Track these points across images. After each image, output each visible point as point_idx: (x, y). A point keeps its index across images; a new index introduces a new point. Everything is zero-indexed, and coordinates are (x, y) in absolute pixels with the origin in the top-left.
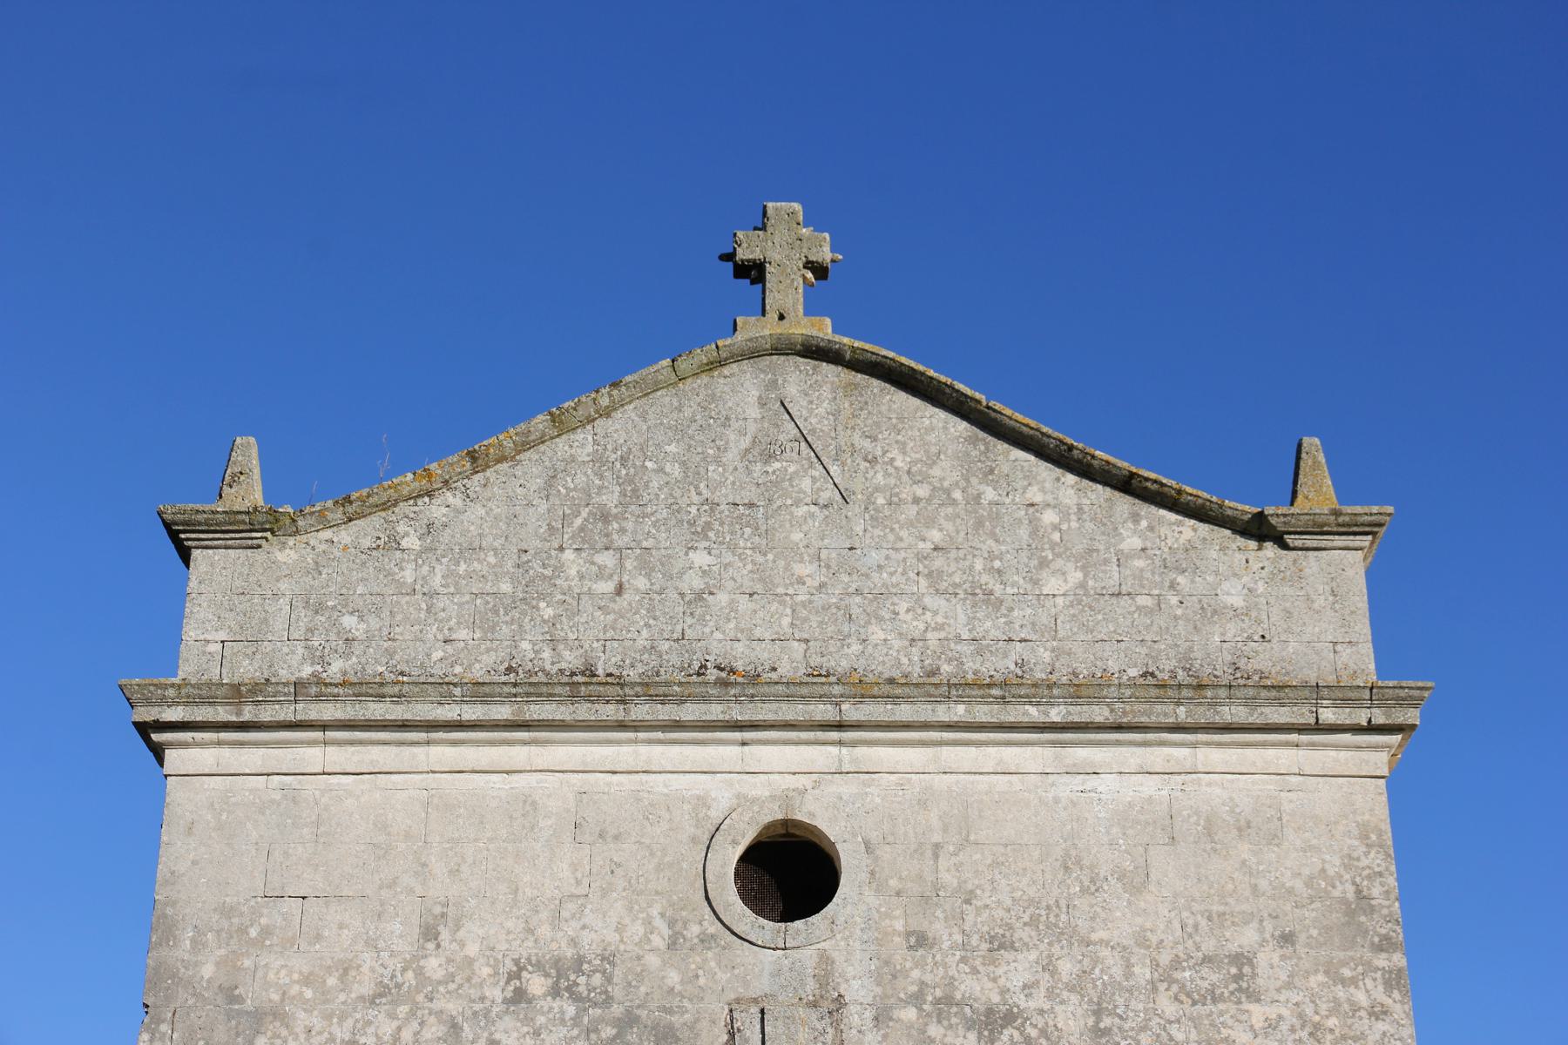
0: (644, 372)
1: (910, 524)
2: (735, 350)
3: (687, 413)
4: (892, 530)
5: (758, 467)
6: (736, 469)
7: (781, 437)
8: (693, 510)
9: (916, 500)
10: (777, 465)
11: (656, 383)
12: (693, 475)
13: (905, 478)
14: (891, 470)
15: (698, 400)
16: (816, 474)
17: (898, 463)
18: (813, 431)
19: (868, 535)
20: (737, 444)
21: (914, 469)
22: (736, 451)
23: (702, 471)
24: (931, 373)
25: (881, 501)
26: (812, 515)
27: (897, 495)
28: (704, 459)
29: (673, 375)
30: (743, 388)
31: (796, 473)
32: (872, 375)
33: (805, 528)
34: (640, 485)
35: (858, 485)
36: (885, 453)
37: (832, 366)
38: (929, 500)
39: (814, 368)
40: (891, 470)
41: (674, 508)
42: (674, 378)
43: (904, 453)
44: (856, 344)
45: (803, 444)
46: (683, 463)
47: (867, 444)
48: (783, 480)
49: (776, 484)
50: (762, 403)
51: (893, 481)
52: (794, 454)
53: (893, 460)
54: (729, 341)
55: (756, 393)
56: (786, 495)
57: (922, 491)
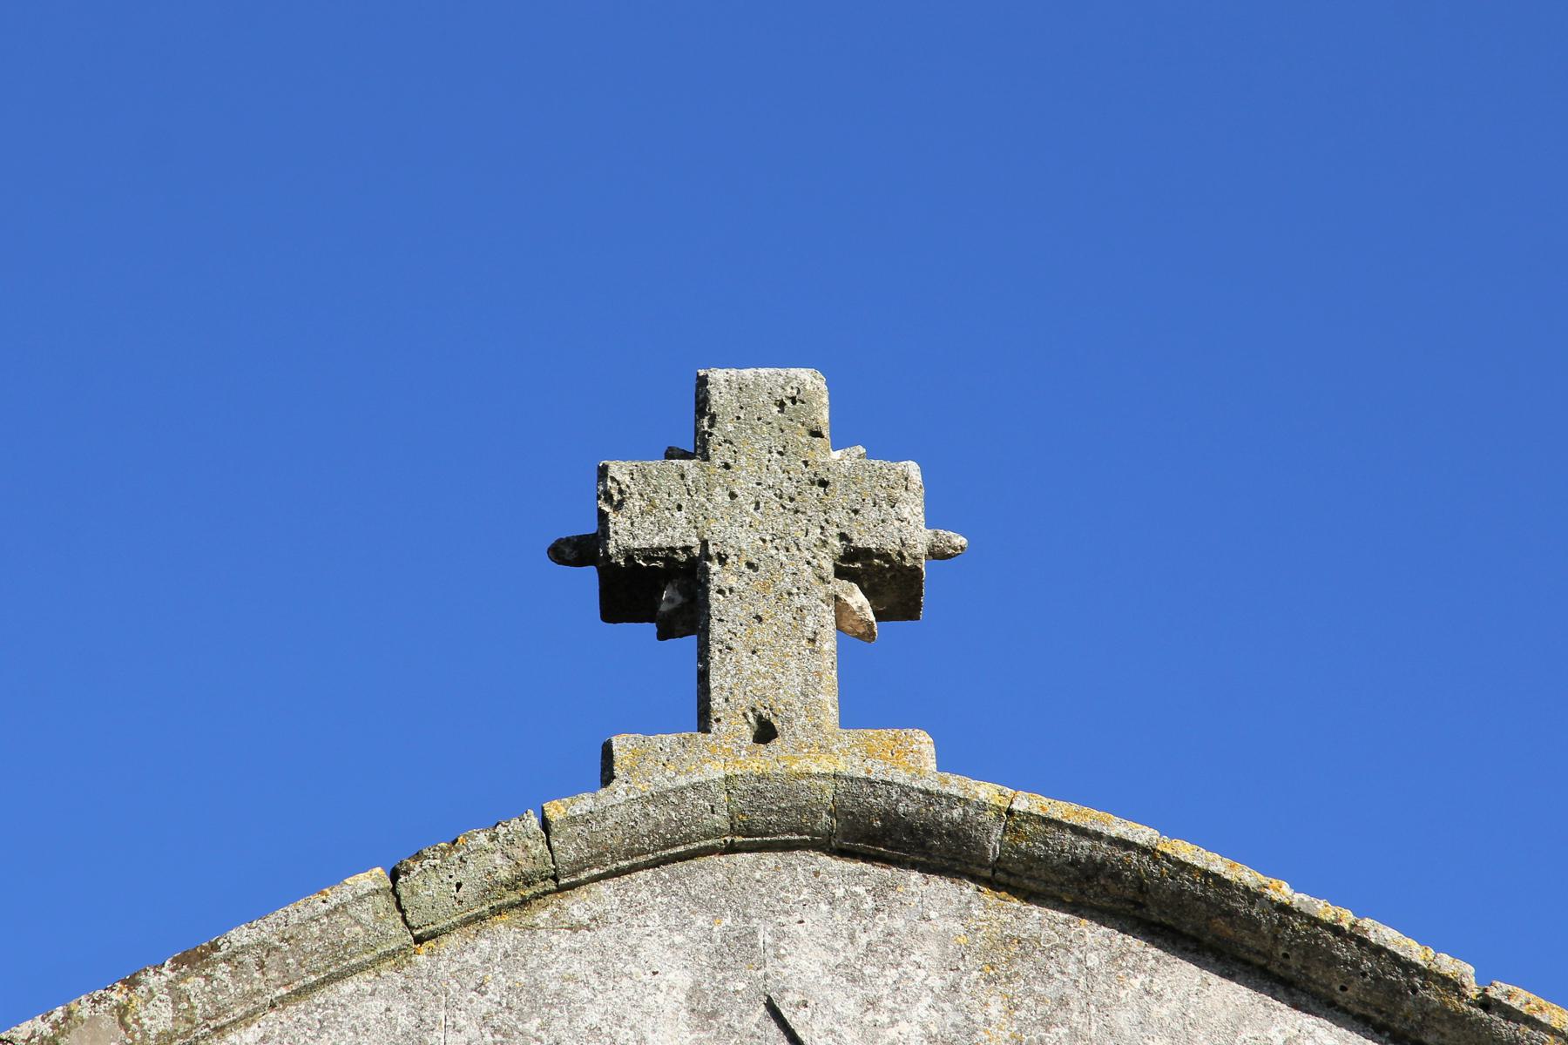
0: (295, 912)
2: (609, 833)
11: (338, 950)
15: (483, 1005)
24: (1283, 892)
37: (941, 886)
39: (879, 892)
42: (398, 936)
54: (584, 804)
55: (684, 980)
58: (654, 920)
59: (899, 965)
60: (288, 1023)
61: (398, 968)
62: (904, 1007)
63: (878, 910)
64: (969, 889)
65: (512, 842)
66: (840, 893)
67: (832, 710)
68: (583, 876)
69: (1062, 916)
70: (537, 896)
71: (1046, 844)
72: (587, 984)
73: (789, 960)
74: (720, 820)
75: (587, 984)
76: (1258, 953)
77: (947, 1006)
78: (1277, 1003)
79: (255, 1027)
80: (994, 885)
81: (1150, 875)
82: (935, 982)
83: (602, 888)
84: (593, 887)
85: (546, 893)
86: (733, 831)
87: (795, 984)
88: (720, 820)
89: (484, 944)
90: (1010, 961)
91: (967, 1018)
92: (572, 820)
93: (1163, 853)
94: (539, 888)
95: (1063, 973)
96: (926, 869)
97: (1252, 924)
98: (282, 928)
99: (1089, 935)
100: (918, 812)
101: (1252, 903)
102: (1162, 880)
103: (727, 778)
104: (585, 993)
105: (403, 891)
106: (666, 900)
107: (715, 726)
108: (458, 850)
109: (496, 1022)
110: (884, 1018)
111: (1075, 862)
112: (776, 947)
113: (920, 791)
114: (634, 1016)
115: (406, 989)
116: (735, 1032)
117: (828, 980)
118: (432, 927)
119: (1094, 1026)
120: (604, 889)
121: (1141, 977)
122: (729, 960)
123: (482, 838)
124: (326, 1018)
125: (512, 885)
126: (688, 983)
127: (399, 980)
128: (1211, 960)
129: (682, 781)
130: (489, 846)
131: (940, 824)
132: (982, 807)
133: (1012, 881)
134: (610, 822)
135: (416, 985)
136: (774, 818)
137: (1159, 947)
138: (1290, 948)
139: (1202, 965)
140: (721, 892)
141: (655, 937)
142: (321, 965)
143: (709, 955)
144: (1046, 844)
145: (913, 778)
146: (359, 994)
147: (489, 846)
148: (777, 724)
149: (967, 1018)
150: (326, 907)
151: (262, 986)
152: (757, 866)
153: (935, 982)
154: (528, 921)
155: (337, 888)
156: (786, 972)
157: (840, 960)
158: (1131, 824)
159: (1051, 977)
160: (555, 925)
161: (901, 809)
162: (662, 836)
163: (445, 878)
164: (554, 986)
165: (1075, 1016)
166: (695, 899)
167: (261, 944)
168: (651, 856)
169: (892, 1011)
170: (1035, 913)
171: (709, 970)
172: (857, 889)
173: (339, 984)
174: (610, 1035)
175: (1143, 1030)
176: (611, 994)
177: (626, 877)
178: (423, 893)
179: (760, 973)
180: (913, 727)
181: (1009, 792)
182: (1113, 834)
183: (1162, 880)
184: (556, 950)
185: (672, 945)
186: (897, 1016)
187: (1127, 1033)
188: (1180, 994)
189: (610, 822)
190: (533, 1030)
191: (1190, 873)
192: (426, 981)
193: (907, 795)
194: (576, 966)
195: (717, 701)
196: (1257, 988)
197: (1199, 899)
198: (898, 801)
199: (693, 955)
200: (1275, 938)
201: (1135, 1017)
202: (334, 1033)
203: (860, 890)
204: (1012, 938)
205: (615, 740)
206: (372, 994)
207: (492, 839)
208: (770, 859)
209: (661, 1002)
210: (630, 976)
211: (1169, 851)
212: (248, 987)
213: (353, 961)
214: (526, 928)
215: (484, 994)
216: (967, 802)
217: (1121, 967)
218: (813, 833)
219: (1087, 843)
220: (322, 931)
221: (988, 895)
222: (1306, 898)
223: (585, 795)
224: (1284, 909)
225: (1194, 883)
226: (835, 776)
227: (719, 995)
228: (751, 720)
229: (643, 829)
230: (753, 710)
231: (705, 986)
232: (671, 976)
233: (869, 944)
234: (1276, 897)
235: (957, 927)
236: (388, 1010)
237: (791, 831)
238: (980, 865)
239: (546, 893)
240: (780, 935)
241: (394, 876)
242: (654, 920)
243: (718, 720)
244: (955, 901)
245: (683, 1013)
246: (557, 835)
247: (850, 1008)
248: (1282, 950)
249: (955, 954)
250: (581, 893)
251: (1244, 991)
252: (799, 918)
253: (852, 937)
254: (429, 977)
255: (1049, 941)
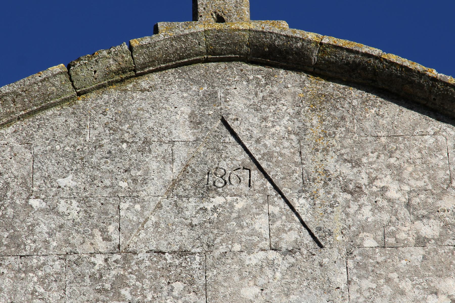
0: (28, 81)
1: (414, 272)
2: (156, 52)
3: (90, 136)
4: (388, 280)
5: (191, 205)
6: (159, 206)
7: (223, 164)
8: (99, 260)
9: (421, 241)
10: (219, 200)
11: (46, 96)
12: (96, 216)
13: (403, 212)
14: (382, 203)
15: (105, 119)
16: (275, 210)
17: (392, 194)
18: (269, 156)
19: (354, 288)
20: (160, 173)
21: (416, 201)
22: (159, 183)
23: (112, 209)
24: (434, 73)
25: (369, 242)
26: (271, 264)
27: (393, 234)
28: (115, 194)
29: (69, 87)
30: (169, 108)
31: (246, 209)
32: (349, 83)
33: (261, 281)
34: (23, 231)
35: (335, 222)
36: (372, 180)
37: (293, 75)
38: (439, 241)
39: (268, 77)
40: (382, 203)
41: (71, 259)
42: (70, 92)
43: (400, 181)
44: (326, 40)
45: (255, 173)
46: (84, 201)
47: (346, 170)
48: (228, 219)
49: (218, 224)
50: (195, 122)
51: (386, 217)
52: (243, 187)
53: (384, 189)
54: (146, 40)
55: (188, 110)
56: (232, 238)
57: (430, 229)
58: (175, 88)
59: (276, 104)
60: (25, 126)
61: (70, 105)
62: (278, 120)
63: (267, 84)
64: (304, 76)
65: (117, 55)
66: (251, 77)
67: (247, 13)
68: (146, 70)
69: (342, 86)
70: (127, 78)
71: (336, 56)
72: (148, 112)
73: (231, 103)
74: (202, 48)
75: (148, 112)
76: (423, 99)
77: (295, 120)
78: (431, 119)
79: (11, 127)
80: (315, 74)
81: (379, 68)
82: (291, 111)
83: (154, 76)
84: (150, 75)
85: (131, 77)
86: (208, 53)
87: (233, 112)
88: (202, 48)
89: (106, 96)
90: (321, 103)
91: (304, 124)
92: (142, 47)
93: (384, 59)
94: (128, 74)
95: (343, 107)
96: (286, 68)
97: (421, 86)
98: (22, 86)
99: (353, 93)
100: (283, 44)
101: (421, 78)
102: (384, 69)
103: (205, 31)
104: (147, 115)
105: (72, 73)
106: (180, 80)
107: (200, 18)
108: (95, 57)
109: (110, 126)
110: (270, 124)
111: (348, 63)
112: (225, 98)
113: (284, 36)
114: (167, 124)
115: (73, 113)
116: (208, 130)
117: (247, 110)
118: (84, 89)
119: (356, 128)
120: (155, 76)
121: (375, 109)
122: (206, 103)
123: (105, 53)
124: (41, 124)
125: (117, 73)
126: (190, 111)
127: (71, 110)
128: (404, 103)
129: (187, 32)
130: (108, 56)
131: (292, 49)
132: (310, 42)
133: (322, 72)
134: (157, 48)
135: (78, 112)
136: (224, 47)
137: (382, 98)
138: (436, 96)
139: (400, 105)
140: (203, 77)
141: (175, 94)
142: (39, 102)
143: (198, 101)
144: (336, 56)
145: (281, 31)
146: (55, 115)
147: (108, 56)
148: (225, 18)
149: (304, 124)
150: (41, 78)
151: (14, 110)
152: (217, 67)
153: (291, 111)
154: (124, 88)
155: (45, 71)
156: (229, 107)
157: (252, 102)
158: (371, 48)
159: (338, 109)
160: (134, 90)
161: (276, 43)
162: (179, 54)
163: (89, 68)
164: (134, 112)
165: (348, 123)
166: (192, 80)
167: (14, 92)
168: (174, 63)
169: (273, 122)
170: (331, 85)
171: (198, 106)
172: (258, 76)
173: (46, 111)
174: (157, 131)
175: (376, 129)
176: (158, 115)
177: (164, 72)
178: (81, 74)
179: (219, 108)
180: (280, 20)
181: (321, 36)
182: (364, 51)
183: (384, 69)
184: (135, 99)
185: (183, 97)
186: (275, 124)
187: (370, 130)
188: (391, 115)
189: (157, 48)
190: (126, 129)
191: (395, 66)
192: (82, 110)
193: (279, 37)
194: (143, 105)
195: (201, 9)
196: (423, 113)
197: (399, 77)
198: (275, 40)
199: (192, 101)
200: (430, 92)
201: (373, 124)
202: (44, 129)
203: (260, 76)
204: (322, 94)
205: (159, 24)
206: (60, 115)
207: (109, 53)
208: (223, 65)
209: (178, 118)
210: (165, 108)
211: (387, 58)
212: (8, 110)
213: (52, 101)
214: (123, 90)
215: (106, 115)
216: (303, 40)
217: (366, 105)
218: (240, 54)
219: (352, 56)
220: (39, 88)
221: (312, 78)
222: (443, 75)
223: (147, 37)
224: (434, 79)
225: (397, 70)
226: (249, 30)
227: (202, 116)
228: (214, 16)
229: (171, 51)
230: (215, 12)
231: (196, 112)
232: (182, 109)
233: (263, 97)
234: (431, 75)
235: (299, 90)
236: (66, 121)
237: (231, 53)
238: (308, 66)
239: (131, 77)
240: (227, 93)
241: (69, 67)
242: (175, 88)
243: (201, 16)
244: (298, 80)
245: (187, 122)
246: (135, 52)
247: (256, 121)
248: (433, 97)
249: (298, 101)
250: (146, 78)
251: (417, 114)
252: (234, 87)
253: (256, 94)
254: (83, 108)
255: (337, 96)
